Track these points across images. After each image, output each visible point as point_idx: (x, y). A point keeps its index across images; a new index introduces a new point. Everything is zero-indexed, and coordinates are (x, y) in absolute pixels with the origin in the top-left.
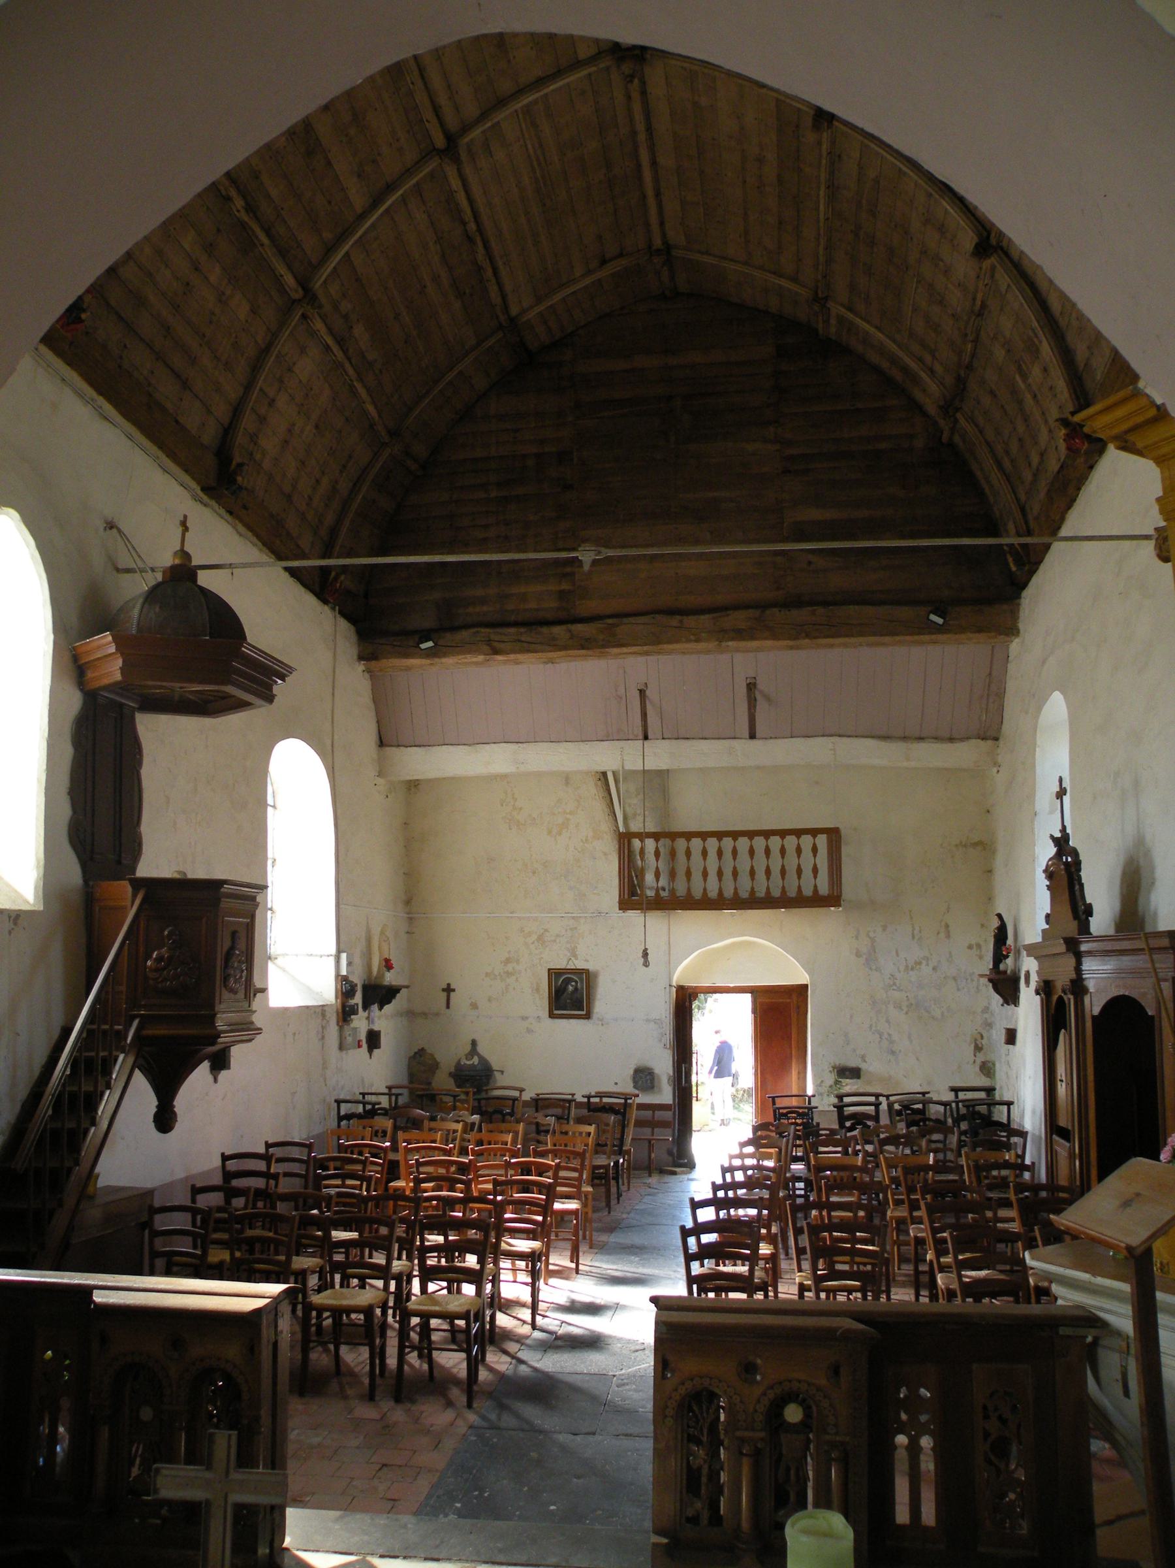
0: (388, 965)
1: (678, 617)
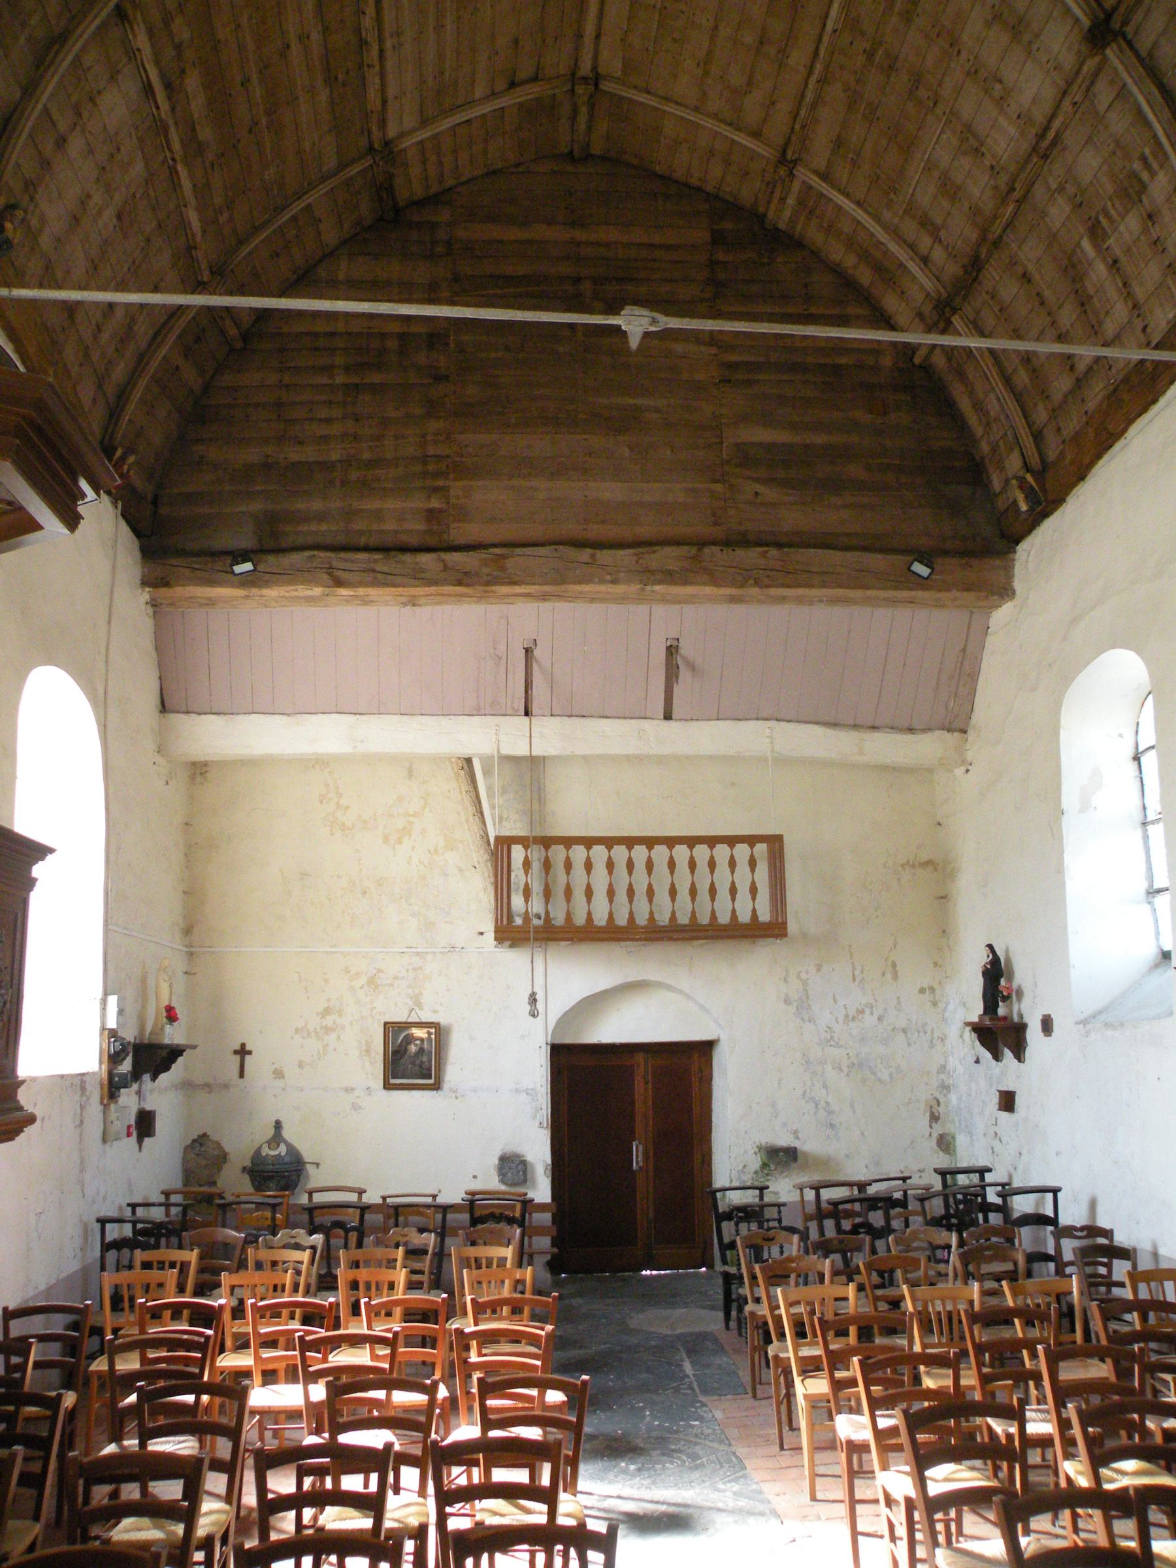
0: (171, 1015)
1: (589, 551)
